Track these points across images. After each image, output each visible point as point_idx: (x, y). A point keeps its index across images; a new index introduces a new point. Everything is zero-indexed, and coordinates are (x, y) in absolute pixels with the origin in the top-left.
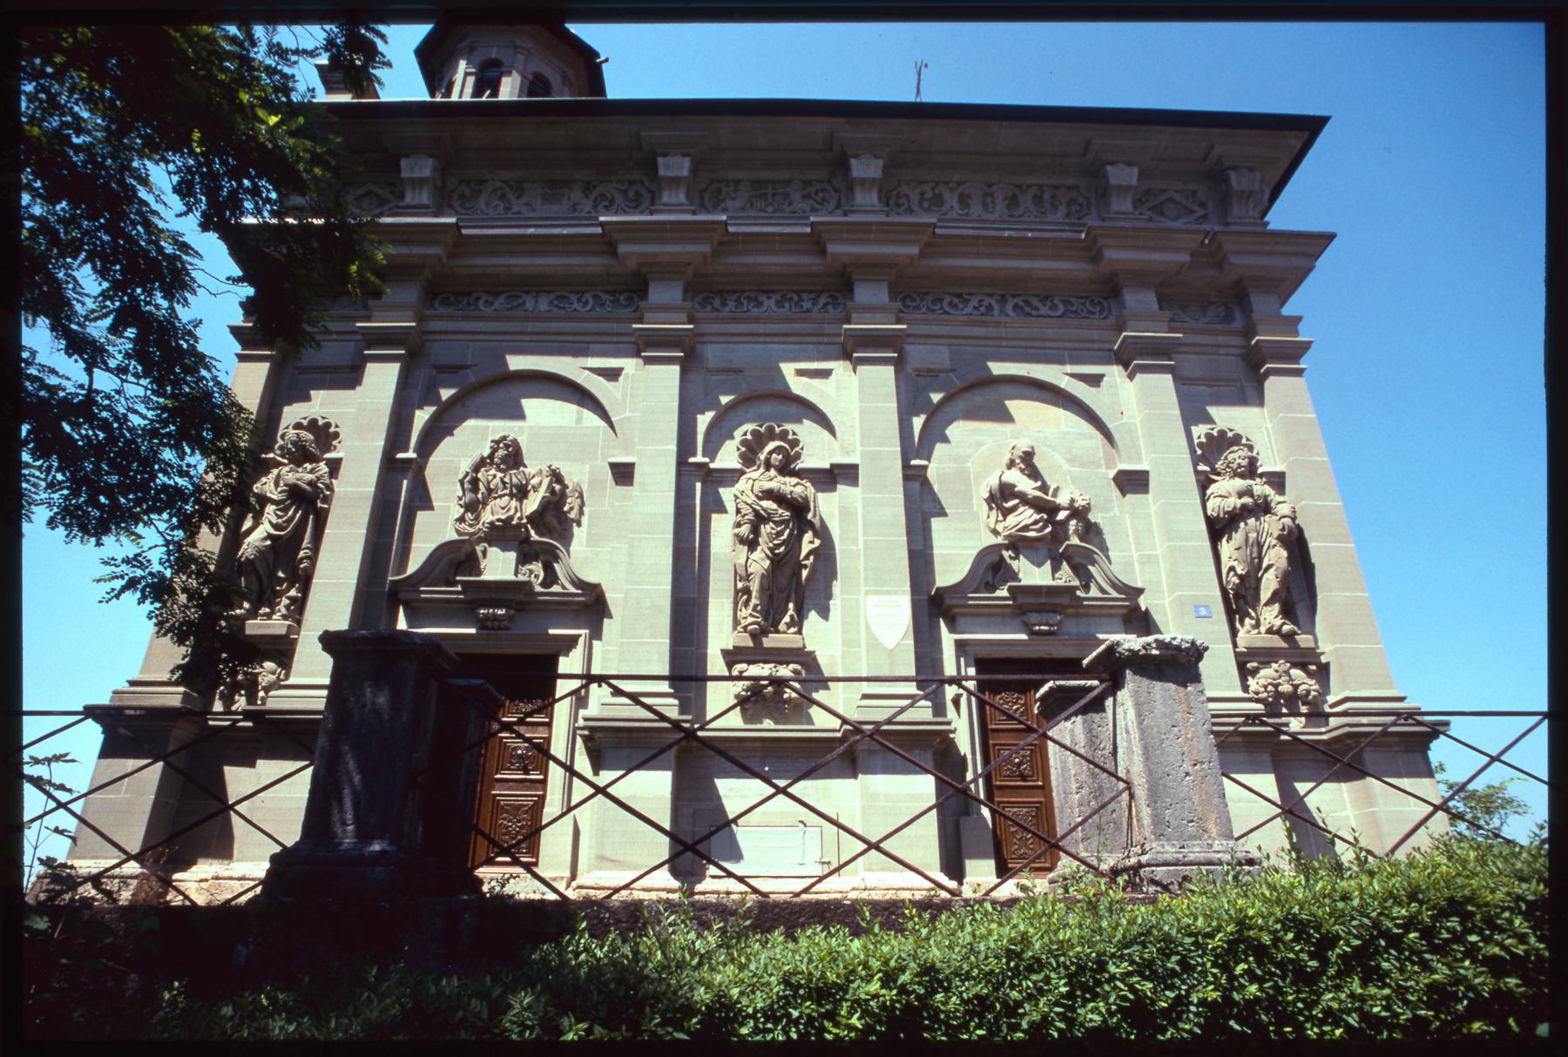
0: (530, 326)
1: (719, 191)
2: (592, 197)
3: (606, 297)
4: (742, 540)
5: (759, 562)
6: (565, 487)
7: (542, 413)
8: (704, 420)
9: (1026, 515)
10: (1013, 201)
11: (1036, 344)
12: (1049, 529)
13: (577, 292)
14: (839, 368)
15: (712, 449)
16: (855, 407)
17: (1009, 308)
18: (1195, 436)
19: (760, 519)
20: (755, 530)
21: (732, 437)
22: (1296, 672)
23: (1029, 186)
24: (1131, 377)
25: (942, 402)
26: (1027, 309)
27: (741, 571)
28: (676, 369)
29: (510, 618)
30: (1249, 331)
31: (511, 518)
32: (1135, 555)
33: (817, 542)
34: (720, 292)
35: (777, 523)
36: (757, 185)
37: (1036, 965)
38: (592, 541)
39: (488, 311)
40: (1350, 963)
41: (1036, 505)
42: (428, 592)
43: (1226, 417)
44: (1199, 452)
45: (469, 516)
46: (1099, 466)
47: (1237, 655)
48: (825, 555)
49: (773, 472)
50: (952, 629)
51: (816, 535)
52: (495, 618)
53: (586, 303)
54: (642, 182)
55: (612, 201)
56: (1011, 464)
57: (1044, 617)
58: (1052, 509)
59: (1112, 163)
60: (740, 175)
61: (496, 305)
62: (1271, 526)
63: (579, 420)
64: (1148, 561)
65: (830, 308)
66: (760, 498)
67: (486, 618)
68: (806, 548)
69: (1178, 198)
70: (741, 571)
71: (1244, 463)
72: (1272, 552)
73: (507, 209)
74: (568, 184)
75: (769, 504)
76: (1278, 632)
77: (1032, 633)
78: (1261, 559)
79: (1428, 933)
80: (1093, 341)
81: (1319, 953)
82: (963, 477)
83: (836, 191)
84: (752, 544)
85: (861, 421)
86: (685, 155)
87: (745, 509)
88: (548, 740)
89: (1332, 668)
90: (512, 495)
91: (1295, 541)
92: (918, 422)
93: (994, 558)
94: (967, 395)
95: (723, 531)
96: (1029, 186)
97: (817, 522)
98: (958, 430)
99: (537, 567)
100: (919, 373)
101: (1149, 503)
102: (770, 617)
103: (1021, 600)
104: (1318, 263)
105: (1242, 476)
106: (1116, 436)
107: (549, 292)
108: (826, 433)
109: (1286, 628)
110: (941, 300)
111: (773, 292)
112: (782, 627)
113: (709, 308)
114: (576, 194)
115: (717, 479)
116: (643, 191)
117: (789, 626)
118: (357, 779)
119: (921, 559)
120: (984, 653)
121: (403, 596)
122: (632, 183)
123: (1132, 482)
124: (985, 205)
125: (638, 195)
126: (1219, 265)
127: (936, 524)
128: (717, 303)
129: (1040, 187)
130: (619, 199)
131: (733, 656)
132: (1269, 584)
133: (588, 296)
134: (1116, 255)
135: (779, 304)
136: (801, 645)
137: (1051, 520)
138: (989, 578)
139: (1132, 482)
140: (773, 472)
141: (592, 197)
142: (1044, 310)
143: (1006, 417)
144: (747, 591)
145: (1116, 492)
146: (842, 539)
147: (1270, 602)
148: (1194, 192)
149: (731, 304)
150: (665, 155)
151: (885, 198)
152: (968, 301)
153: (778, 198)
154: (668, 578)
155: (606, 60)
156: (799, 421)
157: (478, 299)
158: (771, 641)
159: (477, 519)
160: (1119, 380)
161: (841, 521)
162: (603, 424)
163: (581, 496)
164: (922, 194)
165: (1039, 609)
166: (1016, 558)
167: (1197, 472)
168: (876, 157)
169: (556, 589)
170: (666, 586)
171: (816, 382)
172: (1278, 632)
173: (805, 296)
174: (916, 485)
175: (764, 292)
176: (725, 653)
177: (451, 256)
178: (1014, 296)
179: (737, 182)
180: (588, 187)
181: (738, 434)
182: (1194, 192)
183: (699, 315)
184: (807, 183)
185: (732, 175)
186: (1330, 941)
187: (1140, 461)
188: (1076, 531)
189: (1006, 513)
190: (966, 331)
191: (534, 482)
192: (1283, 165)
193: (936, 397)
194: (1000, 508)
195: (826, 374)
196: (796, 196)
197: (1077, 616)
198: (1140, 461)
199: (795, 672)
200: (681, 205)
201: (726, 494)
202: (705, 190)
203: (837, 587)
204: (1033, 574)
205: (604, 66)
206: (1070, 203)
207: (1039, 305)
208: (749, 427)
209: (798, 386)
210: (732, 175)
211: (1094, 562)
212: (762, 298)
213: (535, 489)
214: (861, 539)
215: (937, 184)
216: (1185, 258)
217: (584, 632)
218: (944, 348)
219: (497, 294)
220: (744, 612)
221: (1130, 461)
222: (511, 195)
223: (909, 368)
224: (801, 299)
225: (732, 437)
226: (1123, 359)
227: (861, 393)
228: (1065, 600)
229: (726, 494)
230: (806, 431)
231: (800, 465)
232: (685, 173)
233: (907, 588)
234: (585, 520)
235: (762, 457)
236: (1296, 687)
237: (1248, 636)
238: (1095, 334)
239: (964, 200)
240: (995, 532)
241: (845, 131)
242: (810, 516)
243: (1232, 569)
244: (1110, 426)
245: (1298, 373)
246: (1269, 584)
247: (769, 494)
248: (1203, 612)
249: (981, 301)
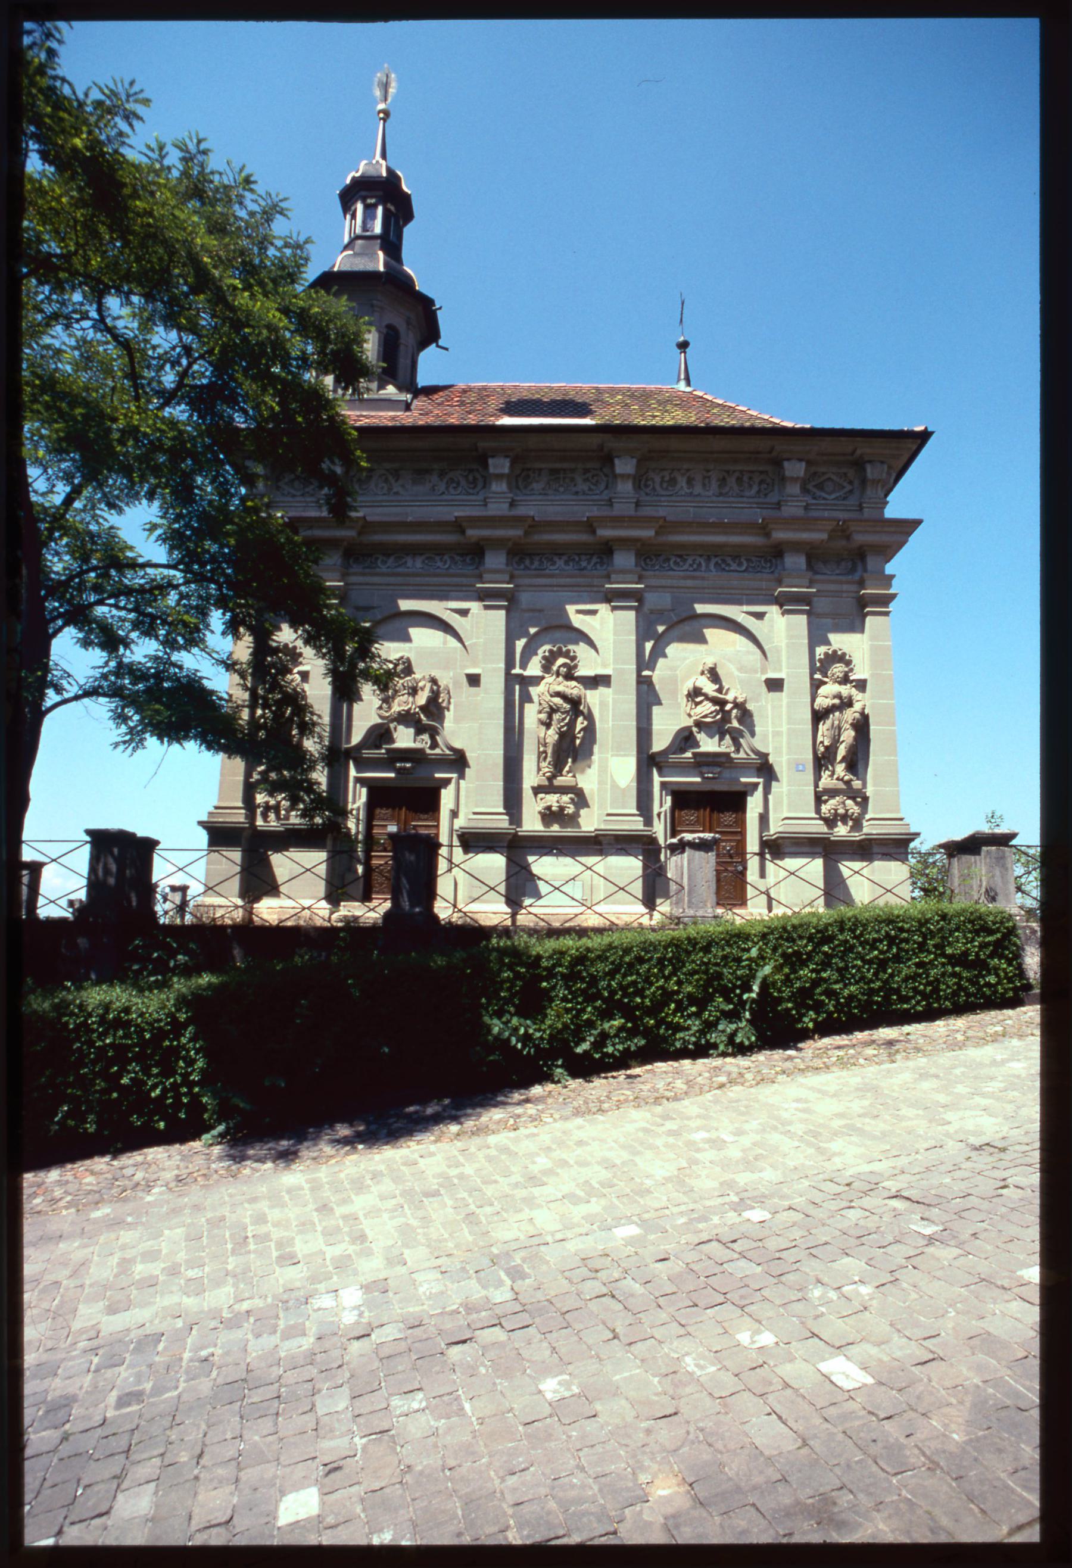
0: (412, 580)
1: (528, 476)
2: (445, 480)
3: (457, 558)
4: (542, 723)
5: (552, 736)
6: (439, 687)
7: (422, 637)
8: (520, 644)
9: (707, 708)
10: (723, 482)
11: (726, 591)
12: (719, 717)
13: (438, 555)
14: (603, 608)
15: (524, 666)
16: (611, 638)
17: (712, 567)
18: (817, 653)
19: (553, 710)
20: (550, 717)
21: (536, 654)
22: (849, 802)
23: (734, 471)
24: (783, 614)
25: (664, 632)
26: (723, 566)
27: (542, 741)
28: (503, 613)
29: (412, 768)
30: (862, 584)
31: (410, 709)
32: (770, 729)
33: (586, 723)
34: (530, 555)
35: (563, 713)
36: (554, 472)
37: (616, 947)
38: (457, 720)
39: (384, 569)
40: (701, 949)
41: (715, 701)
42: (367, 753)
43: (839, 641)
44: (818, 665)
45: (385, 705)
46: (756, 672)
47: (816, 792)
48: (590, 730)
49: (561, 679)
50: (660, 775)
51: (585, 718)
52: (405, 768)
53: (445, 563)
54: (477, 470)
55: (458, 483)
56: (702, 673)
57: (711, 769)
58: (722, 703)
59: (788, 460)
60: (543, 466)
61: (388, 564)
62: (850, 715)
63: (445, 643)
64: (777, 734)
65: (598, 566)
66: (552, 696)
67: (401, 768)
68: (579, 727)
69: (834, 477)
70: (542, 741)
71: (841, 675)
72: (846, 733)
73: (390, 489)
74: (428, 471)
75: (558, 701)
76: (842, 780)
77: (703, 778)
78: (839, 735)
79: (727, 942)
80: (762, 589)
81: (694, 946)
82: (674, 681)
83: (606, 476)
84: (548, 725)
85: (615, 648)
86: (507, 457)
87: (545, 705)
88: (437, 835)
89: (870, 801)
90: (409, 694)
91: (862, 726)
92: (649, 646)
93: (686, 733)
94: (681, 626)
95: (532, 715)
96: (734, 471)
97: (586, 711)
98: (674, 649)
99: (426, 737)
100: (652, 612)
101: (783, 696)
102: (558, 766)
103: (698, 759)
104: (911, 538)
105: (840, 683)
106: (768, 655)
107: (421, 554)
108: (593, 651)
109: (846, 778)
110: (668, 560)
111: (563, 554)
112: (564, 772)
113: (522, 567)
114: (435, 478)
115: (528, 682)
116: (478, 476)
117: (568, 772)
118: (407, 886)
119: (644, 733)
120: (675, 788)
121: (353, 755)
122: (471, 471)
123: (775, 685)
124: (704, 485)
125: (475, 479)
126: (848, 538)
127: (656, 710)
128: (527, 562)
129: (741, 472)
130: (463, 482)
131: (537, 790)
132: (842, 751)
133: (446, 557)
134: (780, 535)
135: (566, 563)
136: (574, 784)
137: (722, 710)
138: (683, 745)
139: (775, 685)
140: (561, 679)
141: (445, 480)
142: (734, 566)
143: (702, 640)
144: (545, 752)
145: (764, 689)
146: (601, 720)
147: (841, 762)
148: (845, 474)
149: (536, 564)
150: (493, 457)
151: (637, 487)
152: (685, 561)
153: (567, 480)
154: (502, 746)
155: (440, 308)
156: (576, 643)
157: (377, 559)
158: (560, 781)
159: (390, 708)
160: (775, 616)
161: (601, 710)
162: (459, 645)
163: (449, 693)
164: (663, 477)
165: (708, 764)
166: (699, 733)
167: (812, 678)
168: (633, 457)
169: (437, 751)
170: (500, 752)
171: (587, 618)
172: (842, 780)
173: (583, 557)
174: (645, 687)
175: (556, 554)
176: (533, 788)
177: (360, 534)
178: (716, 556)
179: (540, 470)
180: (442, 474)
181: (540, 652)
182: (845, 474)
183: (516, 572)
184: (586, 471)
185: (538, 465)
186: (697, 943)
187: (780, 670)
188: (736, 717)
189: (697, 704)
190: (682, 583)
191: (421, 684)
192: (905, 459)
193: (661, 629)
194: (693, 700)
195: (594, 612)
196: (579, 480)
197: (730, 767)
198: (780, 670)
199: (571, 799)
200: (504, 493)
201: (534, 691)
202: (519, 475)
203: (596, 749)
204: (708, 745)
205: (439, 312)
206: (761, 482)
207: (731, 563)
208: (547, 647)
209: (577, 621)
210: (538, 465)
211: (743, 737)
212: (556, 559)
213: (422, 689)
214: (611, 723)
215: (673, 470)
216: (824, 536)
217: (455, 775)
218: (668, 595)
219: (389, 556)
220: (543, 764)
221: (775, 670)
222: (390, 478)
223: (646, 609)
224: (580, 560)
225: (536, 654)
226: (780, 601)
227: (615, 625)
228: (723, 760)
229: (534, 691)
230: (581, 650)
231: (579, 673)
232: (506, 471)
233: (635, 752)
234: (452, 707)
235: (555, 668)
236: (847, 811)
237: (826, 781)
238: (764, 584)
239: (690, 482)
240: (690, 715)
241: (611, 443)
242: (582, 708)
243: (822, 742)
244: (766, 647)
245: (887, 614)
246: (842, 751)
247: (558, 694)
248: (801, 768)
249: (694, 560)
